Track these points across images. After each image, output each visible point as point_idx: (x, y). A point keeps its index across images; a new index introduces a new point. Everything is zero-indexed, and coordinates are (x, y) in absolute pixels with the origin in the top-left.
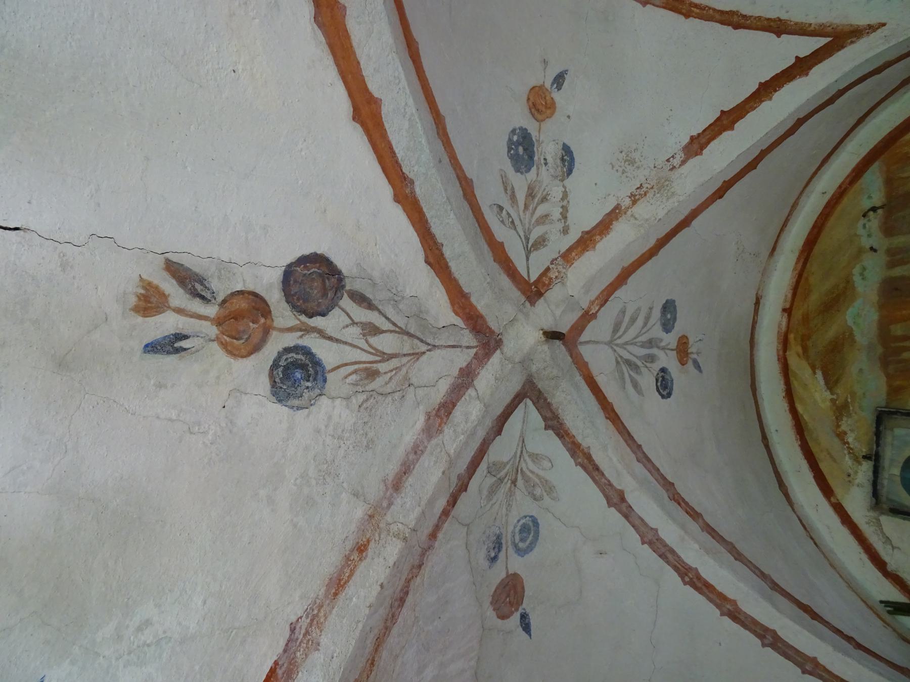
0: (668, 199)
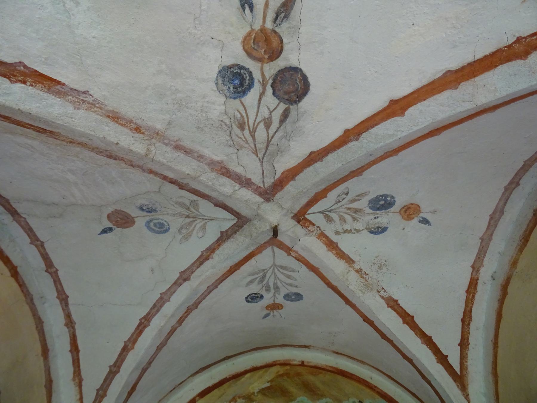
0: (360, 290)
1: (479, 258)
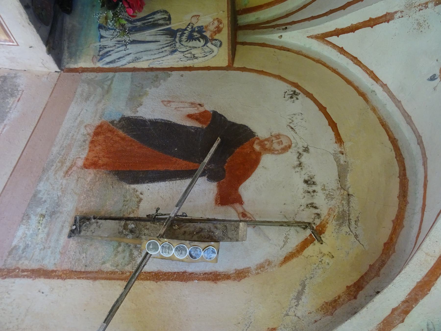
1: (389, 92)
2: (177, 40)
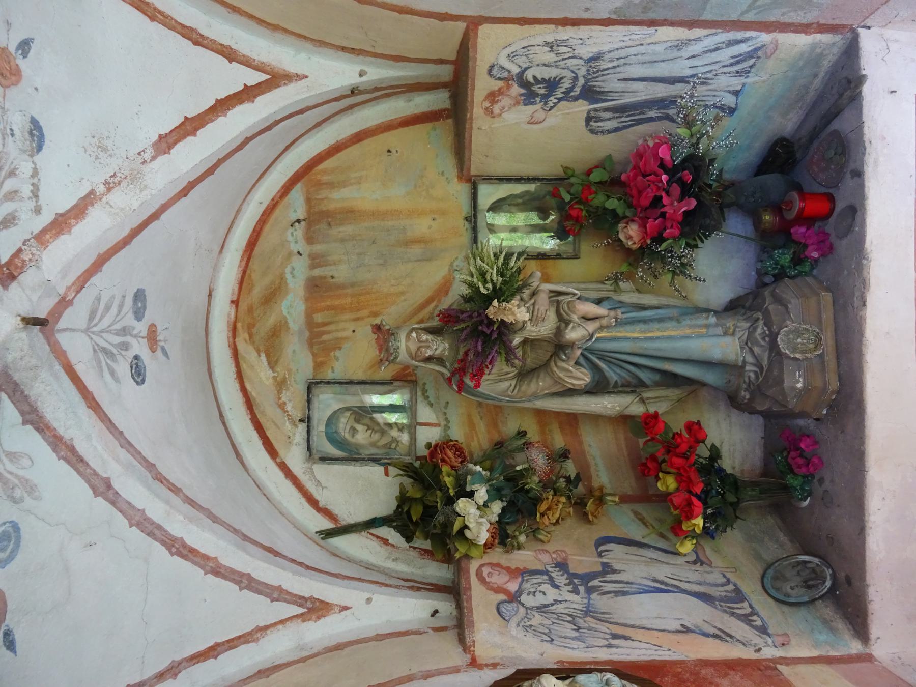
0: (141, 191)
2: (581, 81)
